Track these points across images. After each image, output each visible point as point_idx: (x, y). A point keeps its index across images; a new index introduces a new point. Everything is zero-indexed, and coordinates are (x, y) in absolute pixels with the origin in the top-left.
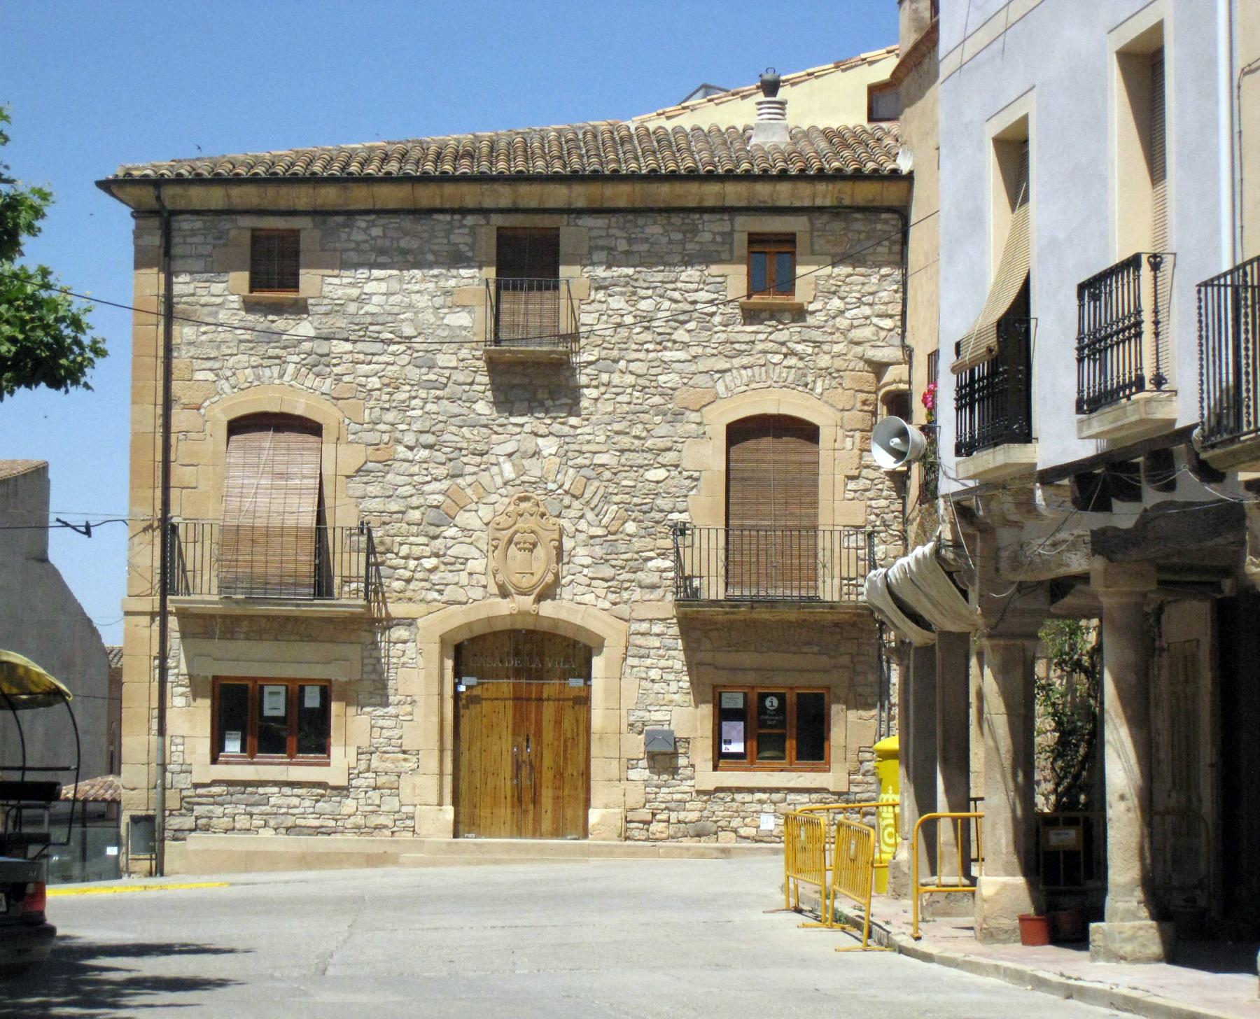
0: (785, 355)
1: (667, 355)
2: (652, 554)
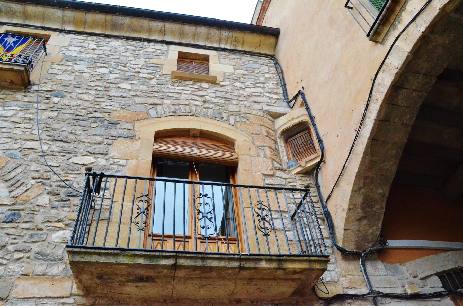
0: (205, 102)
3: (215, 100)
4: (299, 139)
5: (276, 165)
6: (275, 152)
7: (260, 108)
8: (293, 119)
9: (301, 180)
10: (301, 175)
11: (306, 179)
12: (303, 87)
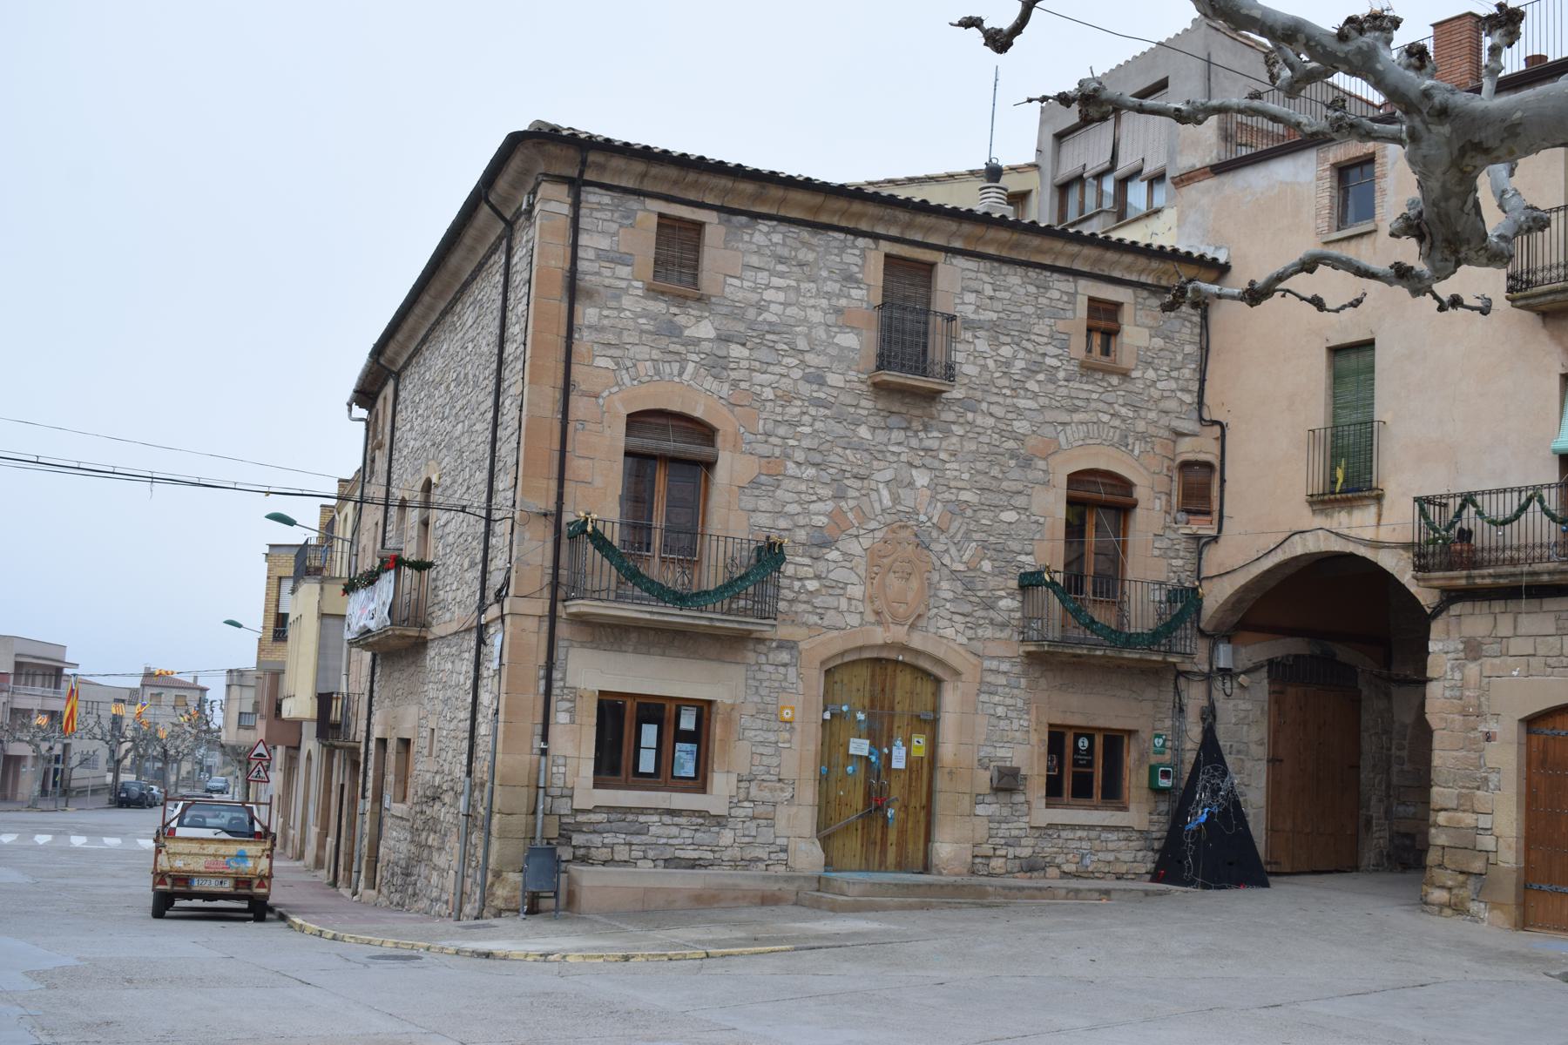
1: (1022, 403)
2: (1003, 593)
3: (1123, 411)
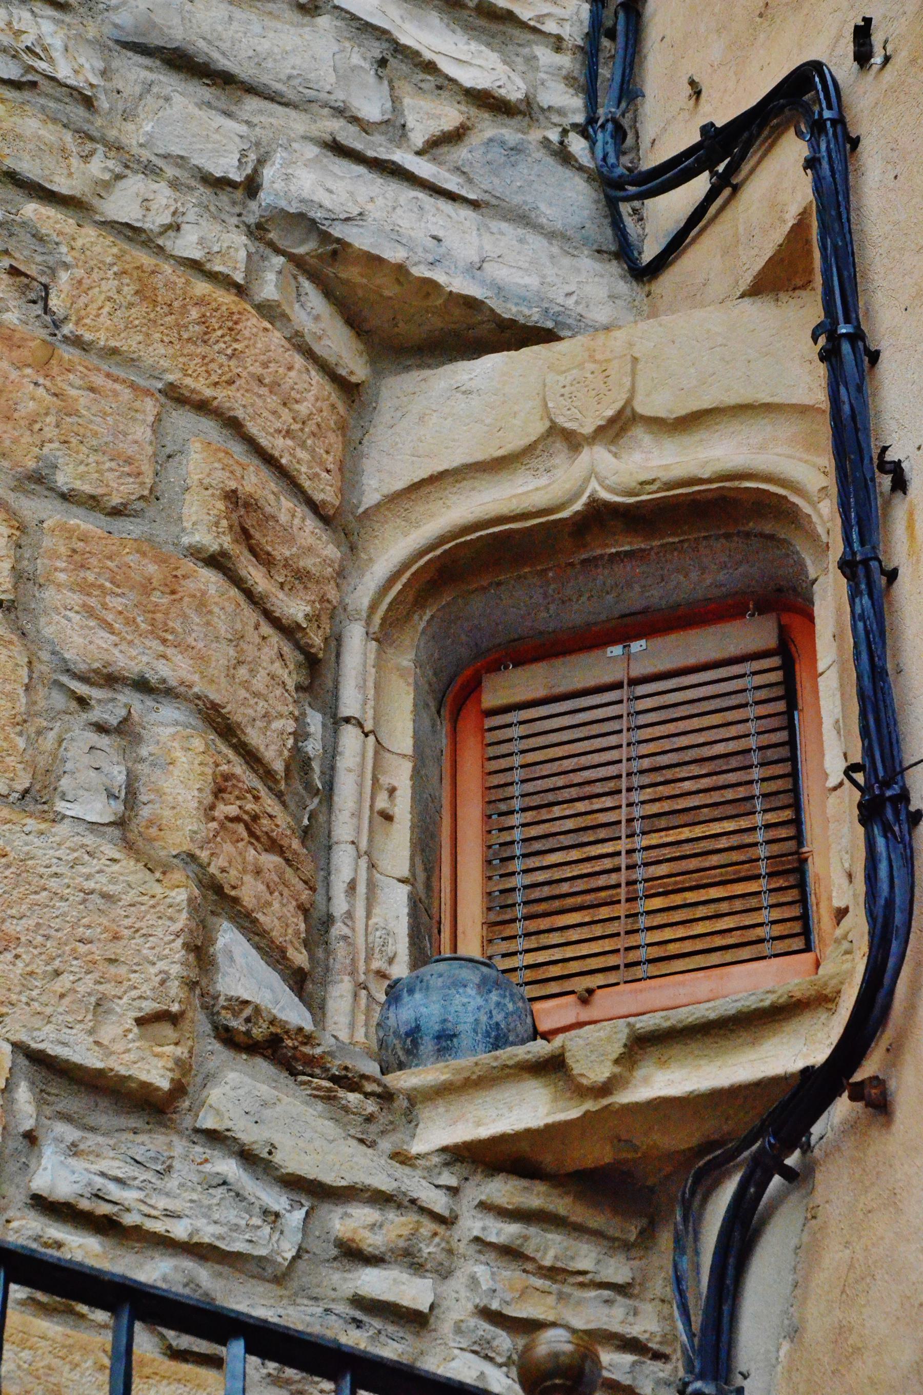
4: (626, 706)
5: (245, 976)
6: (282, 797)
7: (226, 165)
8: (619, 426)
9: (510, 1253)
10: (535, 1197)
11: (585, 1257)
12: (863, 34)
